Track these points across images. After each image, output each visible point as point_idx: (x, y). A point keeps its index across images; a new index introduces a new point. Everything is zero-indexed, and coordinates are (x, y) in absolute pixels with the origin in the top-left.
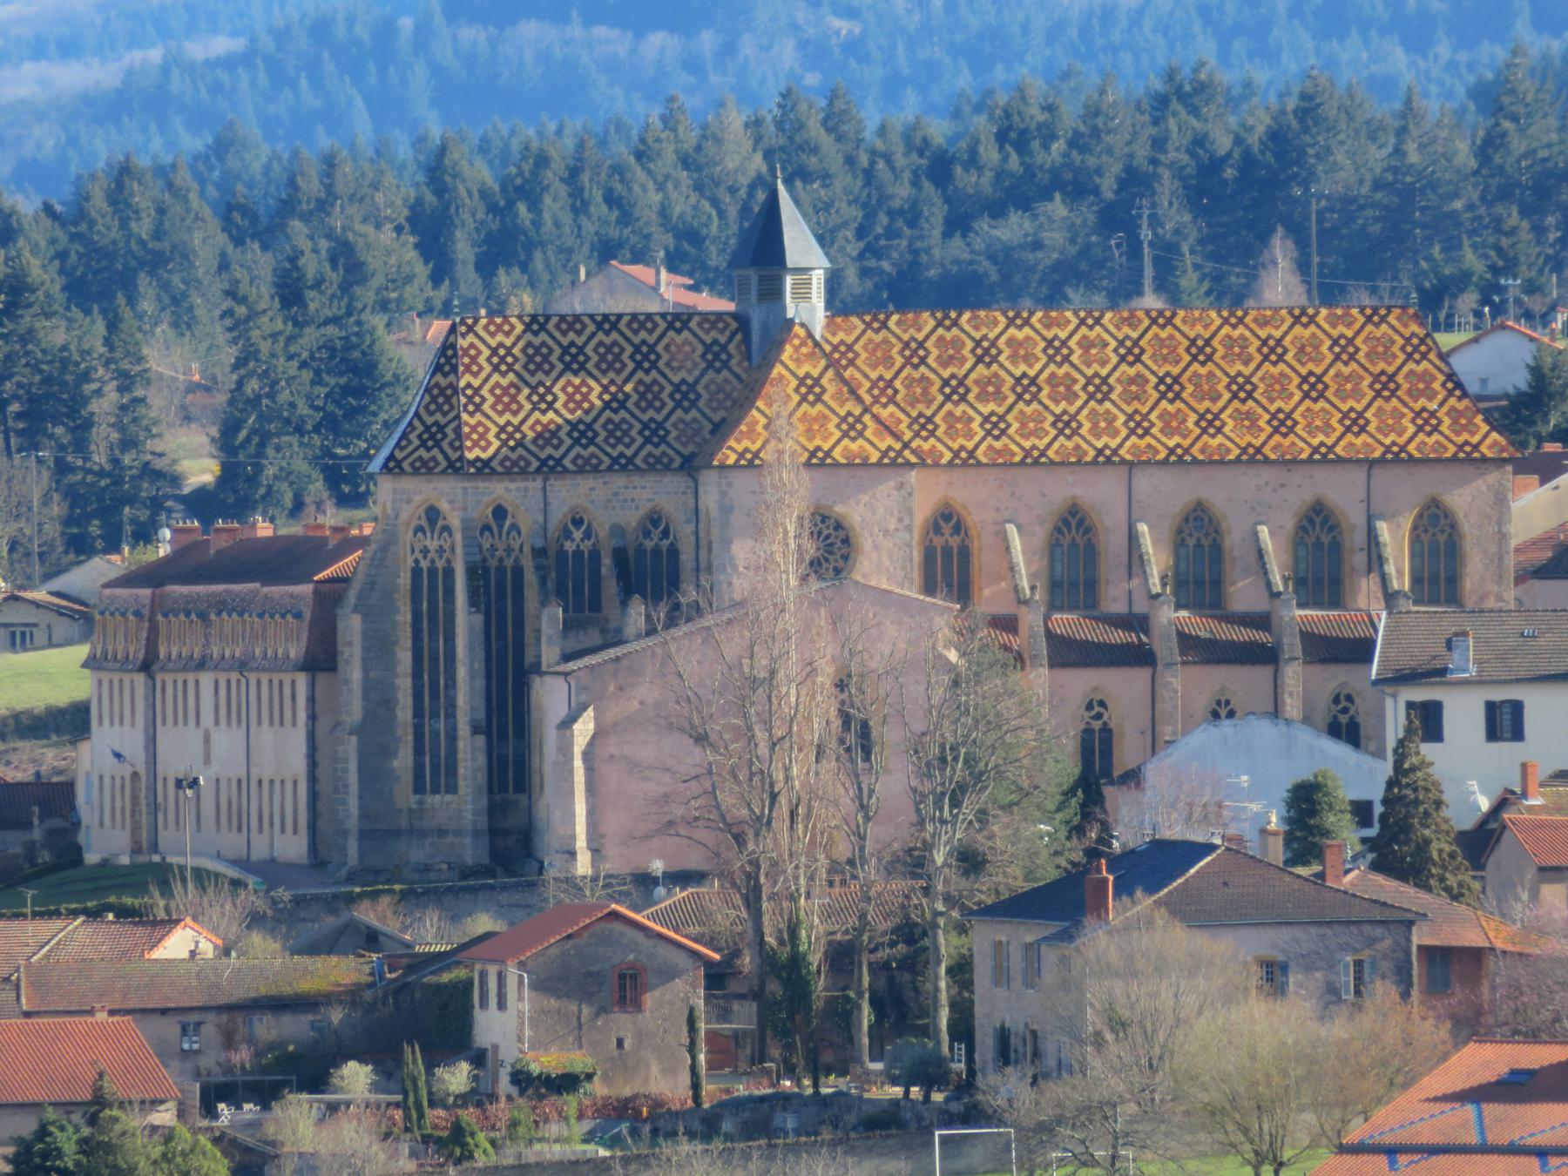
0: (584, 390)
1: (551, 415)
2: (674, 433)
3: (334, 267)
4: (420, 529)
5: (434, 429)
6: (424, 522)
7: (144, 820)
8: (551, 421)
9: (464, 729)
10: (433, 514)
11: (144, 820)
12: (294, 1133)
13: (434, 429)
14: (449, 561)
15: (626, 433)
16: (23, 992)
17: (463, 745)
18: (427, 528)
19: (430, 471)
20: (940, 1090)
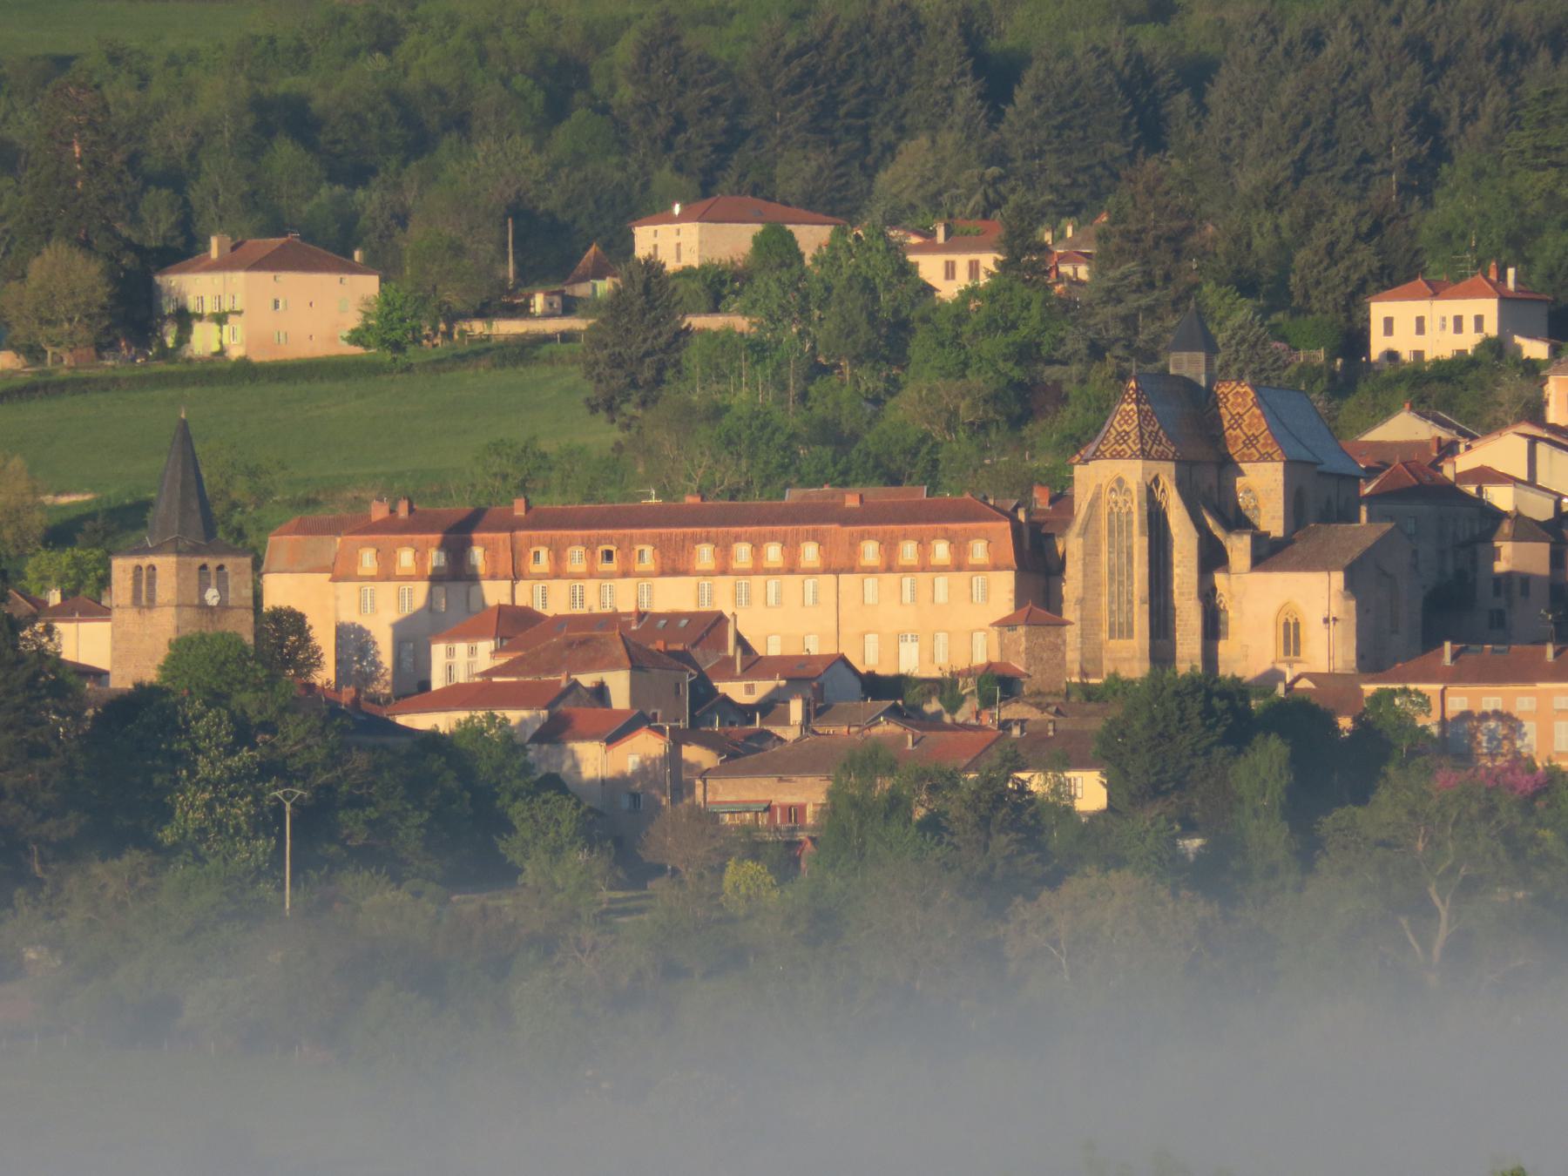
0: (1123, 414)
1: (1132, 435)
2: (1125, 427)
3: (1037, 213)
4: (1112, 490)
5: (1235, 426)
6: (1115, 485)
7: (144, 587)
8: (1135, 434)
9: (1136, 602)
10: (1120, 481)
11: (144, 587)
12: (1183, 29)
13: (1235, 426)
14: (1130, 508)
15: (1126, 422)
16: (93, 603)
17: (1136, 609)
18: (1117, 488)
19: (1121, 457)
20: (1089, 272)
